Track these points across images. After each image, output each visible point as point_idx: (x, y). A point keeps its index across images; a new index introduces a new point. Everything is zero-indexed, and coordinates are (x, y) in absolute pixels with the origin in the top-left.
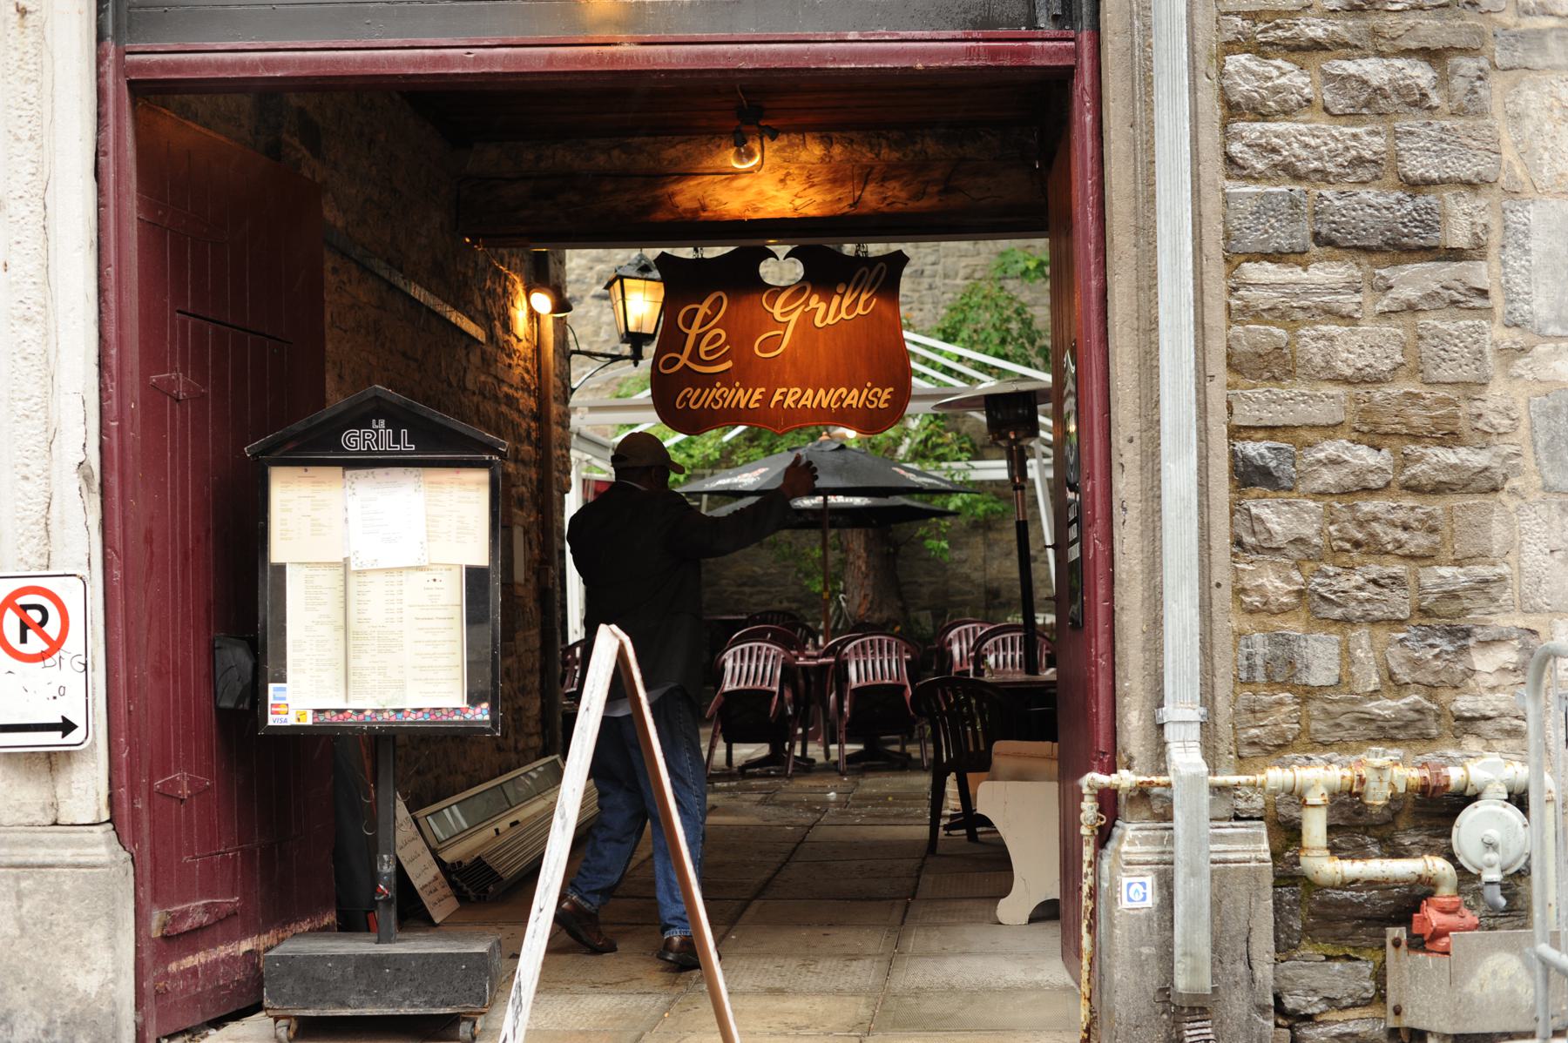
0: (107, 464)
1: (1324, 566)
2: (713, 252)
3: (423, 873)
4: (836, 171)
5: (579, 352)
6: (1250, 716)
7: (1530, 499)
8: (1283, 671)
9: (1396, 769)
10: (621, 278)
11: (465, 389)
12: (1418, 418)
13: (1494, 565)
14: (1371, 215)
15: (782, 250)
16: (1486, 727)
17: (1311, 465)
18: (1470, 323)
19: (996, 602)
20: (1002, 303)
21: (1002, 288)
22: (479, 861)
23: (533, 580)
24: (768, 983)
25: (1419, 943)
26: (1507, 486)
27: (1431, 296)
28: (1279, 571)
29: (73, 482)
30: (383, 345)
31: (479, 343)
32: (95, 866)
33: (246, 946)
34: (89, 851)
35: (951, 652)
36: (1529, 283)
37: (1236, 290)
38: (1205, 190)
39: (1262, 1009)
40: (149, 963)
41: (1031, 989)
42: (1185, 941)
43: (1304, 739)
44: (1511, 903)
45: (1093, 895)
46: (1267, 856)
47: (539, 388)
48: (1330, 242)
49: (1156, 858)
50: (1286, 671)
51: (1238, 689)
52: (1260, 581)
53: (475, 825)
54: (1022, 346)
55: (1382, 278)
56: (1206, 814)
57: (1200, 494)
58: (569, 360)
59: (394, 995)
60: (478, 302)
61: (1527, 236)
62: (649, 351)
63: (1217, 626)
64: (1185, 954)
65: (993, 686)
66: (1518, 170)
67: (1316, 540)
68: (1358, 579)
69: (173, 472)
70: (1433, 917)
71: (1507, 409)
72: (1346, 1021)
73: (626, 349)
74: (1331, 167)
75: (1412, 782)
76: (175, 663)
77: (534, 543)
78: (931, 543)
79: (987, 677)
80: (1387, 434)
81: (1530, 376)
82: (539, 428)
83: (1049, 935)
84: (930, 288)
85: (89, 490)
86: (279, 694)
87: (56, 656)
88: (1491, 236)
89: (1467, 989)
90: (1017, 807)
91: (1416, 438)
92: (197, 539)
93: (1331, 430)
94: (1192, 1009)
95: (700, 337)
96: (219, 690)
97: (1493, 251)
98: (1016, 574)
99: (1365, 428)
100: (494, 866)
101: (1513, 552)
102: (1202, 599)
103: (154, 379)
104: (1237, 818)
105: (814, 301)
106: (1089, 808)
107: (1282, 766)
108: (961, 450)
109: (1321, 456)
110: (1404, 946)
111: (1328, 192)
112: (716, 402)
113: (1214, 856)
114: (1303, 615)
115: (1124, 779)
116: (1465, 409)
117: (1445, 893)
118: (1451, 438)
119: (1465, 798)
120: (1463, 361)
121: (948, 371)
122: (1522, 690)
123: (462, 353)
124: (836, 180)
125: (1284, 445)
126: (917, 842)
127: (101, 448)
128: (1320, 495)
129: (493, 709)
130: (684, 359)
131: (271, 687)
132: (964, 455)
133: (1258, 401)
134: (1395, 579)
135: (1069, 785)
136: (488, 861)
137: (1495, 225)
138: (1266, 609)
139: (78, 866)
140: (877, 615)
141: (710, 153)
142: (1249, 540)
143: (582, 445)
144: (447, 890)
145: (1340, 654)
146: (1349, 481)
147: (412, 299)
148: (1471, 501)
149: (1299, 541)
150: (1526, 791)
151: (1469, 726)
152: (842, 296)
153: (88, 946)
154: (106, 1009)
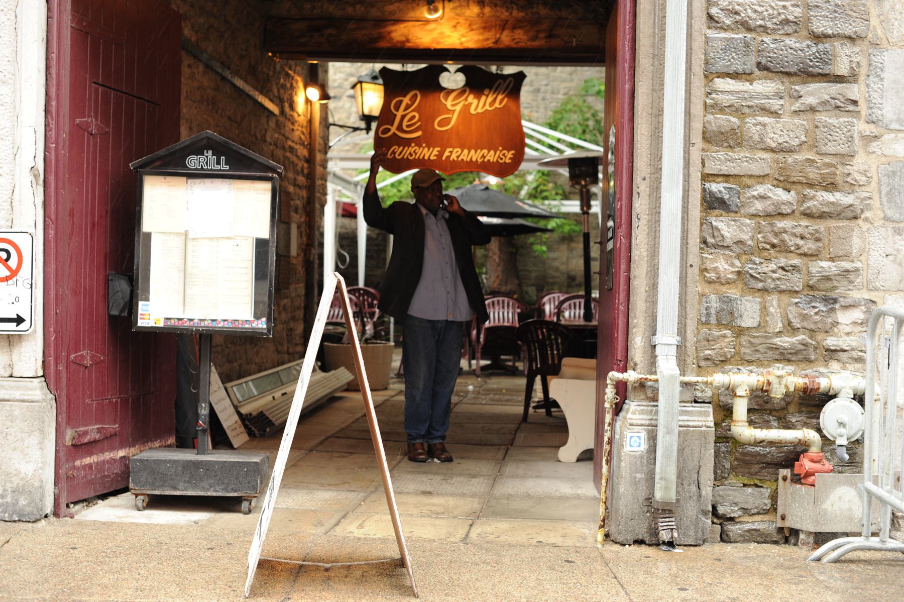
0: (48, 169)
1: (753, 258)
2: (411, 67)
3: (228, 420)
4: (486, 23)
5: (334, 125)
6: (706, 343)
7: (876, 224)
8: (727, 318)
9: (789, 377)
10: (361, 82)
11: (265, 141)
12: (813, 174)
13: (853, 262)
14: (792, 54)
15: (452, 67)
16: (843, 356)
17: (749, 198)
18: (846, 119)
19: (573, 284)
20: (585, 110)
21: (585, 101)
22: (261, 415)
23: (302, 255)
24: (423, 488)
25: (797, 479)
26: (862, 216)
27: (824, 103)
28: (727, 258)
29: (28, 178)
30: (217, 112)
31: (275, 115)
32: (33, 402)
33: (121, 453)
34: (30, 392)
35: (544, 311)
36: (882, 97)
37: (710, 94)
38: (695, 34)
39: (705, 513)
40: (63, 459)
41: (574, 498)
42: (662, 471)
43: (737, 358)
44: (852, 457)
45: (610, 442)
46: (712, 424)
47: (310, 144)
48: (767, 69)
49: (647, 422)
50: (729, 318)
51: (700, 327)
52: (716, 265)
53: (262, 393)
54: (595, 135)
55: (796, 91)
56: (677, 398)
57: (683, 212)
58: (328, 128)
59: (205, 484)
60: (275, 91)
61: (882, 70)
62: (374, 125)
63: (689, 290)
64: (661, 479)
65: (565, 327)
66: (879, 32)
67: (750, 242)
68: (773, 266)
69: (88, 177)
70: (806, 464)
71: (865, 171)
72: (753, 522)
73: (363, 125)
74: (769, 25)
75: (798, 386)
76: (85, 287)
77: (304, 234)
78: (537, 247)
79: (563, 322)
80: (794, 182)
81: (879, 152)
82: (309, 167)
83: (587, 468)
84: (544, 99)
85: (37, 183)
86: (145, 308)
87: (14, 279)
88: (861, 69)
89: (824, 507)
90: (572, 392)
91: (811, 185)
92: (101, 217)
93: (761, 178)
94: (664, 510)
95: (403, 117)
96: (111, 305)
97: (862, 78)
98: (582, 268)
99: (782, 178)
100: (270, 417)
101: (864, 254)
102: (681, 273)
103: (78, 121)
104: (696, 402)
105: (471, 99)
106: (610, 392)
107: (723, 373)
108: (557, 194)
109: (755, 193)
110: (789, 480)
111: (767, 39)
112: (411, 155)
113: (681, 423)
114: (740, 286)
115: (631, 376)
116: (841, 170)
117: (814, 450)
118: (831, 187)
119: (829, 396)
120: (841, 142)
121: (551, 147)
122: (865, 335)
123: (264, 120)
124: (486, 28)
125: (733, 186)
126: (517, 415)
127: (45, 159)
128: (753, 216)
129: (268, 321)
130: (393, 129)
131: (141, 303)
132: (559, 197)
133: (720, 159)
134: (795, 267)
135: (601, 382)
136: (267, 413)
137: (864, 63)
138: (718, 281)
139: (23, 401)
141: (413, 9)
142: (710, 240)
143: (336, 181)
144: (243, 428)
145: (761, 309)
146: (771, 209)
147: (235, 86)
148: (841, 224)
149: (740, 242)
150: (864, 394)
151: (833, 355)
152: (487, 96)
153: (28, 447)
154: (37, 484)
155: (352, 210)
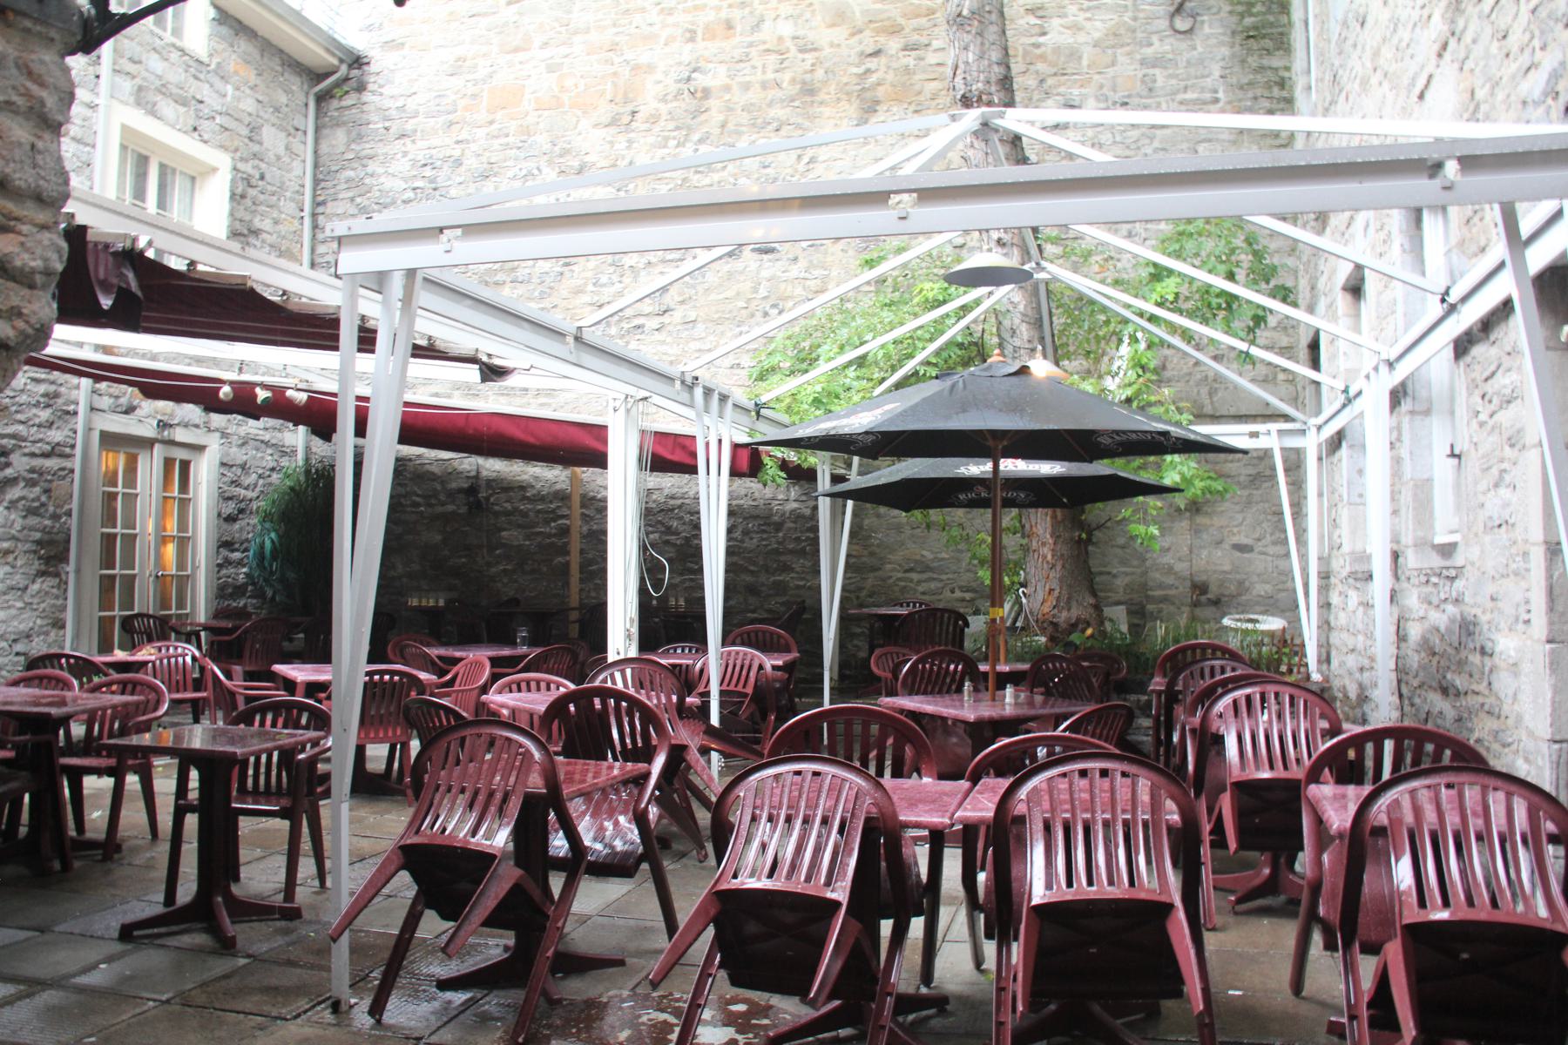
78: (1138, 529)
98: (105, 826)
140: (1064, 614)
155: (589, 441)
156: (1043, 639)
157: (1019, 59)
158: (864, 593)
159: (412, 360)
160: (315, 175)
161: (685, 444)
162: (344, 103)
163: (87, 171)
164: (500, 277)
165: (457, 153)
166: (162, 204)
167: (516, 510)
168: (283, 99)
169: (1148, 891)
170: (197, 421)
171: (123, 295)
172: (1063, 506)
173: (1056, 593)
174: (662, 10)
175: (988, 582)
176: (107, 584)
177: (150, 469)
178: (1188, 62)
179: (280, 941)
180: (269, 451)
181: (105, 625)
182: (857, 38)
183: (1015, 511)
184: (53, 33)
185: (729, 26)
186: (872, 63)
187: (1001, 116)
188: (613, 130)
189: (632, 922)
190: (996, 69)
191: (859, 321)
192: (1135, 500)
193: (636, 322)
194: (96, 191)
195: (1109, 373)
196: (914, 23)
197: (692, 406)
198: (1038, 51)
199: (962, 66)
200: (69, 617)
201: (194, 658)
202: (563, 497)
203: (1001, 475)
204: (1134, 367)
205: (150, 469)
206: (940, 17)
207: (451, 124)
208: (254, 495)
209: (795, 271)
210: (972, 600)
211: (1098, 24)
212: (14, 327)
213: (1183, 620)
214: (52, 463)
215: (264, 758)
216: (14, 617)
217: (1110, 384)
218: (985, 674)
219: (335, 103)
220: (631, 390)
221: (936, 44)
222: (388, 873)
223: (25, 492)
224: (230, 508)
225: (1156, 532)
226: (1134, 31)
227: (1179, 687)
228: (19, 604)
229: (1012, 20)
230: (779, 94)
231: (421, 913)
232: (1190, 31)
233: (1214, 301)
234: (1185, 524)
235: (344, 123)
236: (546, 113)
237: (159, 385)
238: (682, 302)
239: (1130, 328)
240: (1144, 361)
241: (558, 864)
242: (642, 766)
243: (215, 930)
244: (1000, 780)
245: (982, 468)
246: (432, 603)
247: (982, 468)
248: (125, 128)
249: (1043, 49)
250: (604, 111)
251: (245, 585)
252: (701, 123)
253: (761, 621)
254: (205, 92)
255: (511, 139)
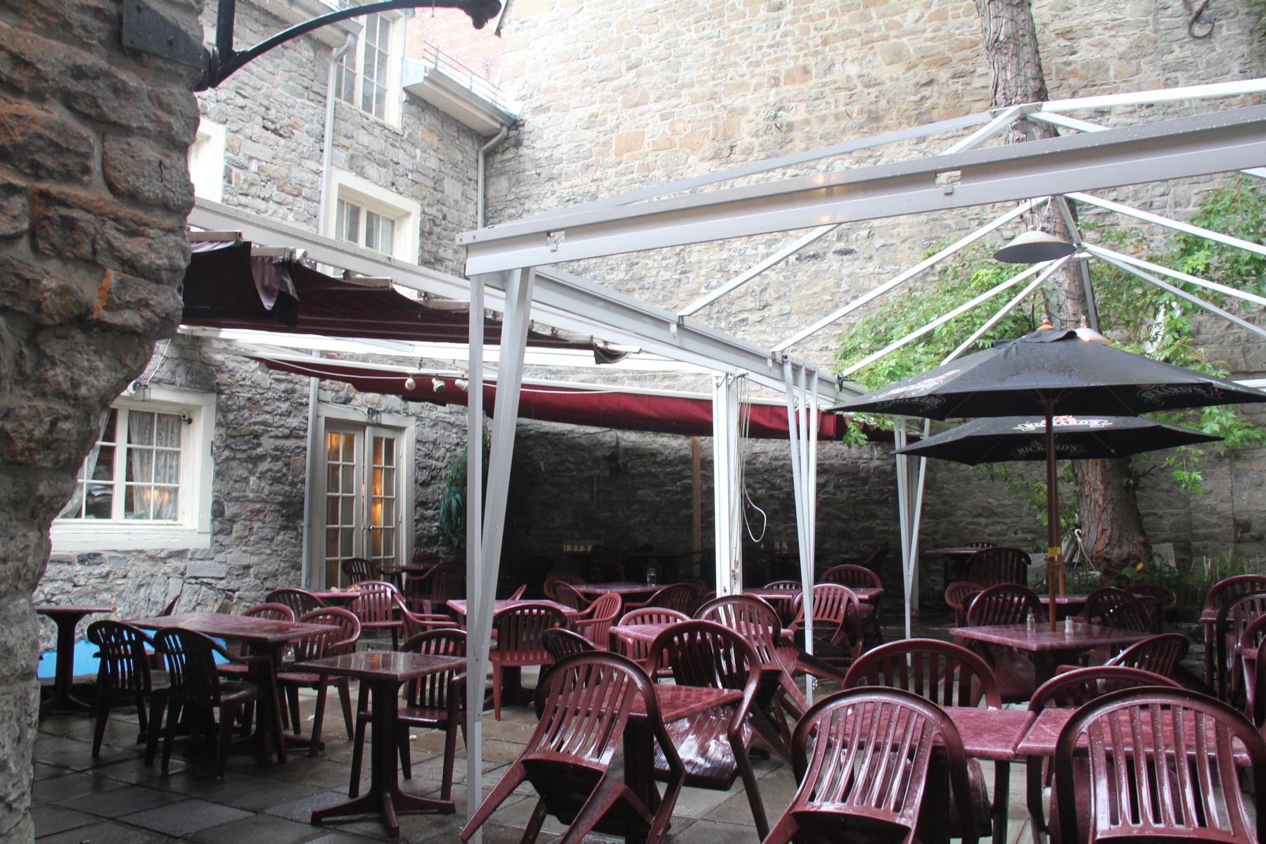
140: (1116, 551)
155: (698, 412)
156: (1098, 573)
157: (1053, 76)
158: (939, 535)
159: (528, 349)
160: (485, 214)
161: (778, 412)
162: (506, 157)
163: (314, 221)
164: (631, 285)
165: (593, 189)
166: (369, 242)
167: (648, 472)
168: (459, 157)
169: (1220, 831)
170: (398, 408)
171: (282, 298)
172: (1108, 455)
173: (1108, 532)
174: (751, 64)
175: (1046, 524)
176: (332, 536)
177: (363, 446)
178: (1208, 63)
179: (435, 832)
180: (454, 430)
181: (331, 566)
182: (912, 72)
183: (1068, 462)
184: (181, 71)
185: (806, 71)
186: (926, 92)
187: (1038, 109)
188: (716, 162)
189: (730, 827)
190: (1032, 83)
191: (925, 305)
192: (1178, 449)
193: (742, 316)
194: (321, 233)
195: (1148, 339)
196: (960, 55)
197: (782, 380)
198: (1069, 68)
199: (1001, 84)
200: (304, 560)
201: (393, 593)
202: (686, 461)
203: (1054, 430)
204: (1169, 332)
205: (363, 446)
206: (982, 46)
207: (588, 167)
208: (443, 465)
209: (870, 268)
210: (1033, 540)
211: (1122, 39)
212: (142, 317)
213: (1228, 556)
214: (290, 443)
215: (438, 675)
216: (265, 561)
217: (1150, 348)
218: (1046, 605)
219: (499, 158)
220: (731, 369)
221: (980, 70)
222: (512, 784)
223: (271, 466)
224: (424, 476)
225: (1199, 477)
226: (1155, 42)
227: (1230, 618)
228: (268, 551)
229: (1045, 45)
230: (851, 123)
231: (543, 818)
232: (1209, 35)
233: (1244, 269)
234: (1226, 469)
235: (506, 173)
236: (662, 153)
237: (368, 381)
238: (779, 298)
239: (1165, 298)
240: (1179, 325)
241: (662, 776)
242: (736, 692)
243: (384, 821)
244: (1061, 710)
245: (1037, 425)
246: (582, 549)
247: (1037, 425)
248: (341, 187)
249: (1074, 66)
250: (708, 148)
251: (437, 536)
252: (787, 152)
253: (852, 561)
254: (400, 156)
255: (635, 175)
